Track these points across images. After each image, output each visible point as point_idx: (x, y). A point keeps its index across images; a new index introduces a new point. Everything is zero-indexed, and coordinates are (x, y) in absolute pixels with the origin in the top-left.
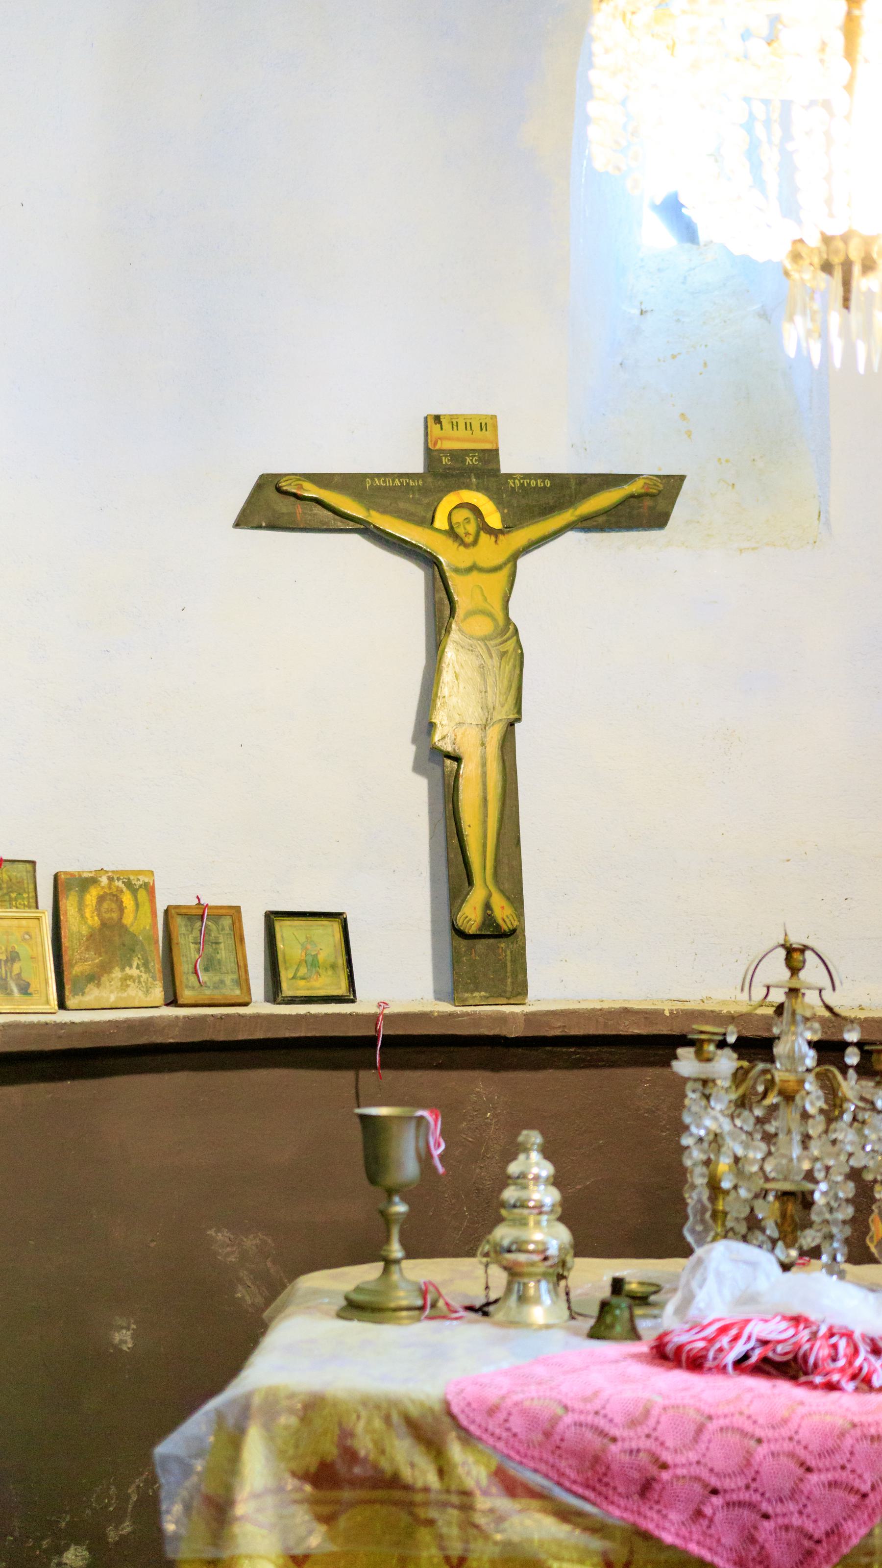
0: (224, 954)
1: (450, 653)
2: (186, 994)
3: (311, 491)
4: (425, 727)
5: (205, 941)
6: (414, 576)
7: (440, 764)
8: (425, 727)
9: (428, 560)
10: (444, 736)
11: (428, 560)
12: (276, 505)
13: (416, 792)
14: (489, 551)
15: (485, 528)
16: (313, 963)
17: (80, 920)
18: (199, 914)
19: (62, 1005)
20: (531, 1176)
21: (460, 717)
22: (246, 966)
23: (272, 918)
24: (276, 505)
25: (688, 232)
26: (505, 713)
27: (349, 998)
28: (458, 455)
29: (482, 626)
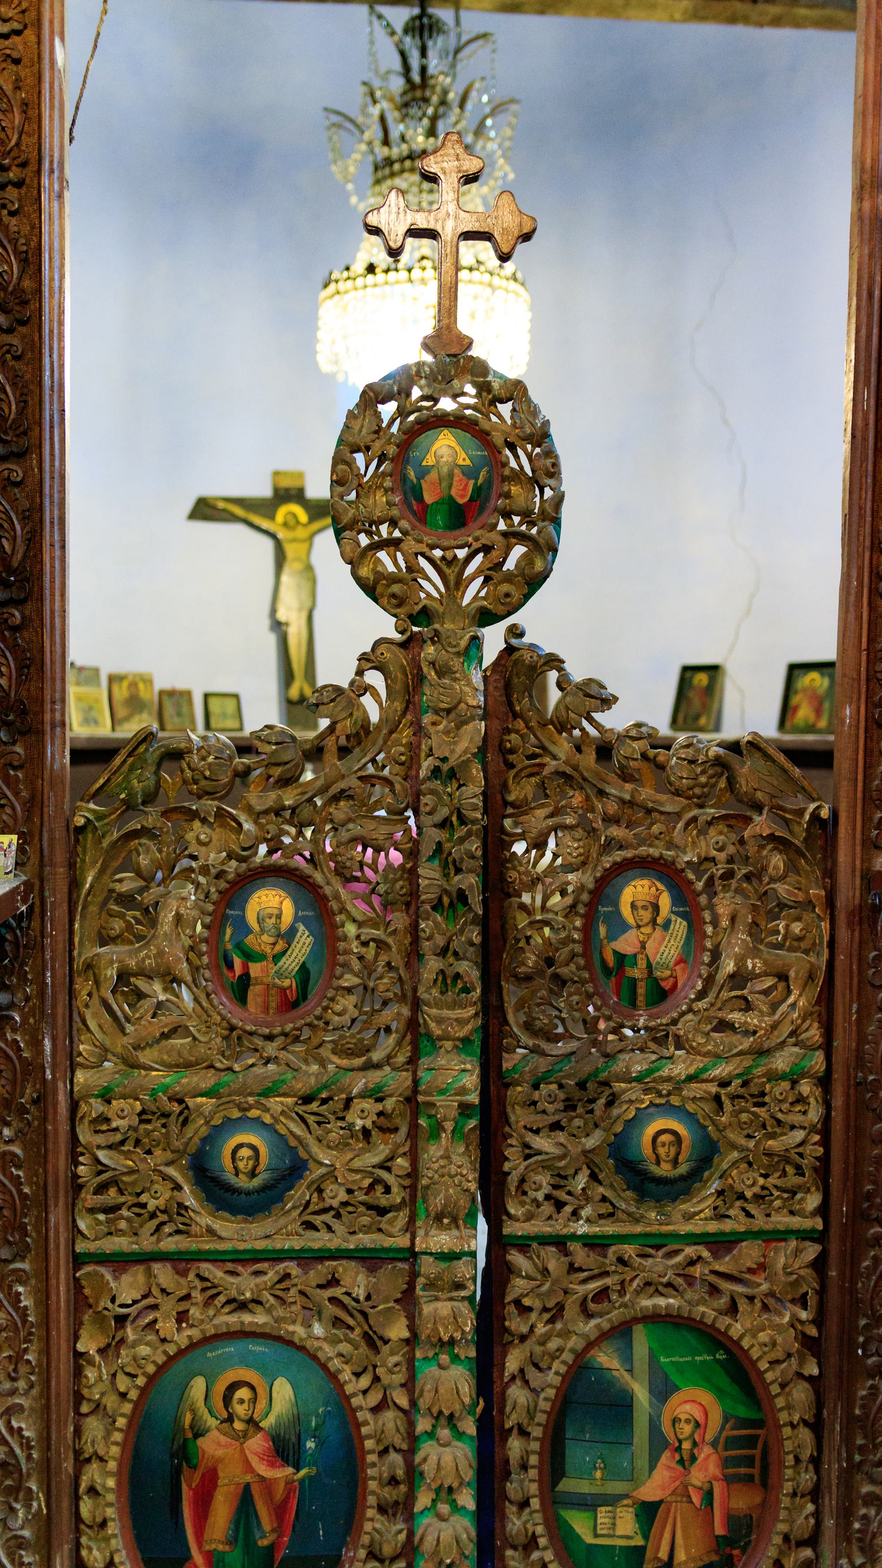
0: (185, 709)
1: (285, 578)
2: (169, 726)
3: (221, 505)
4: (273, 611)
5: (178, 706)
6: (268, 545)
7: (278, 627)
8: (273, 611)
9: (273, 536)
10: (282, 616)
11: (273, 536)
12: (205, 510)
13: (271, 640)
14: (302, 533)
15: (298, 522)
16: (224, 715)
17: (121, 692)
18: (172, 693)
19: (113, 729)
20: (437, 626)
21: (290, 612)
22: (63, 477)
23: (206, 696)
24: (205, 510)
25: (431, 234)
26: (308, 605)
27: (241, 729)
28: (287, 490)
29: (298, 566)
